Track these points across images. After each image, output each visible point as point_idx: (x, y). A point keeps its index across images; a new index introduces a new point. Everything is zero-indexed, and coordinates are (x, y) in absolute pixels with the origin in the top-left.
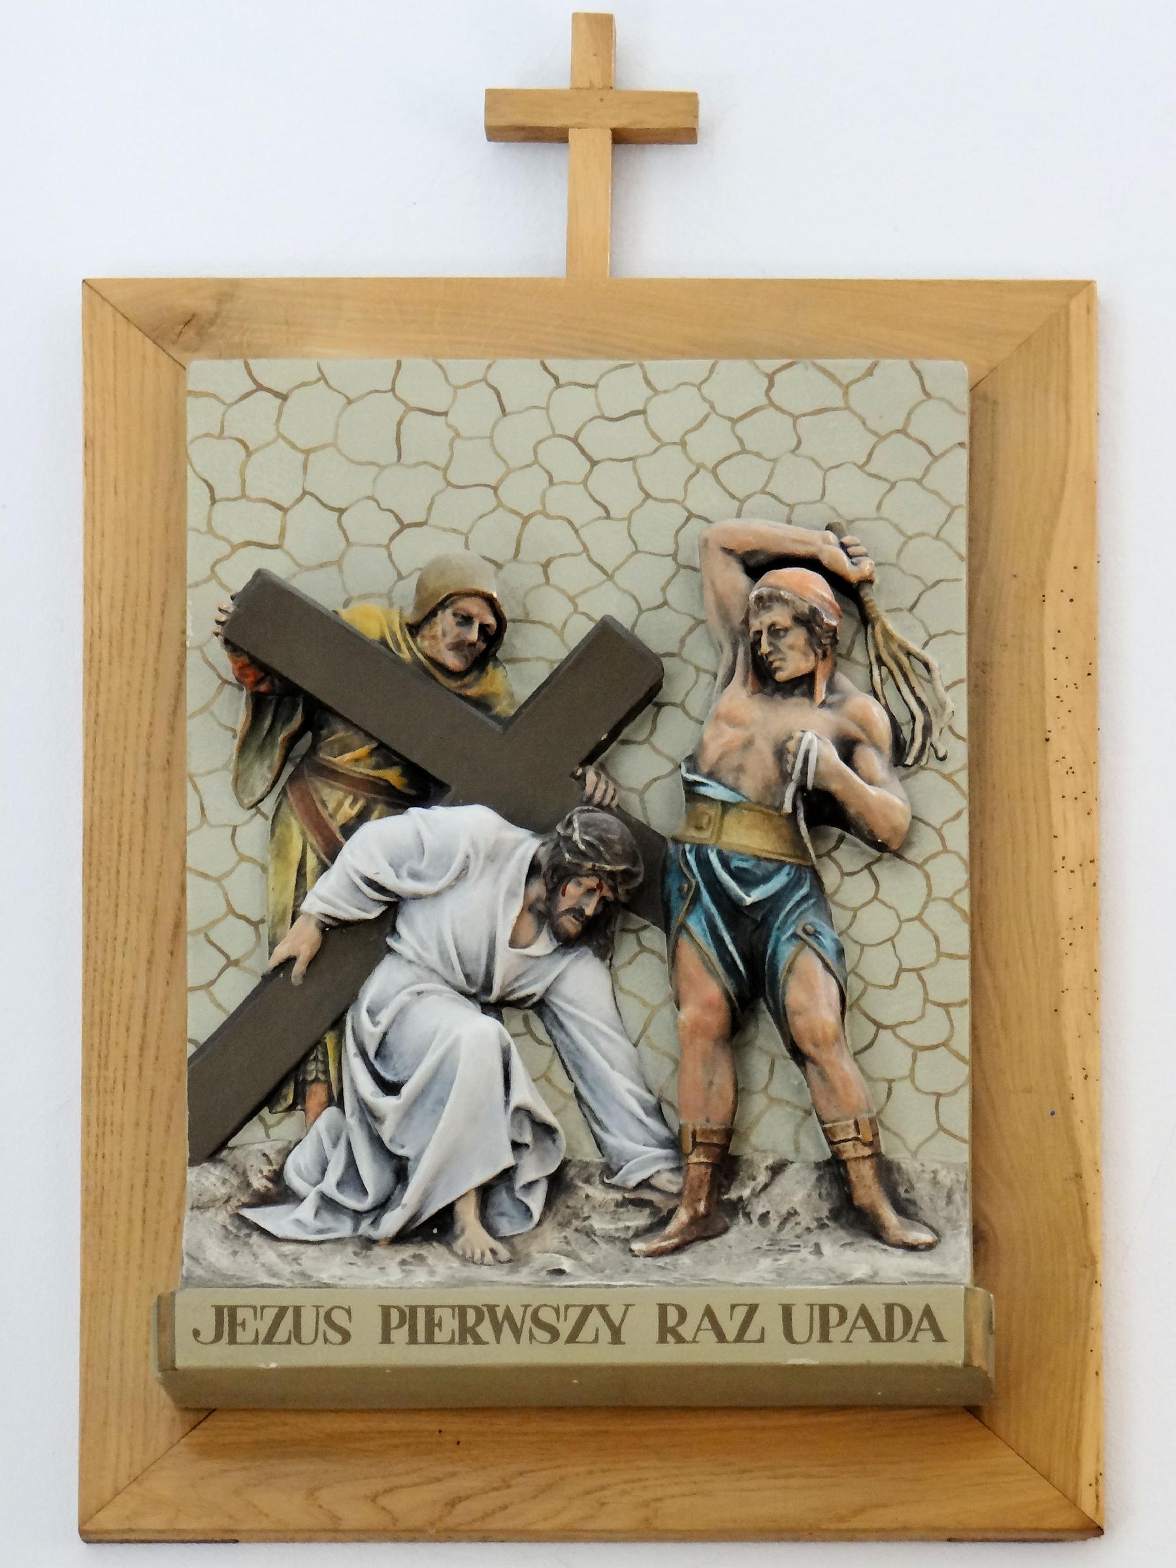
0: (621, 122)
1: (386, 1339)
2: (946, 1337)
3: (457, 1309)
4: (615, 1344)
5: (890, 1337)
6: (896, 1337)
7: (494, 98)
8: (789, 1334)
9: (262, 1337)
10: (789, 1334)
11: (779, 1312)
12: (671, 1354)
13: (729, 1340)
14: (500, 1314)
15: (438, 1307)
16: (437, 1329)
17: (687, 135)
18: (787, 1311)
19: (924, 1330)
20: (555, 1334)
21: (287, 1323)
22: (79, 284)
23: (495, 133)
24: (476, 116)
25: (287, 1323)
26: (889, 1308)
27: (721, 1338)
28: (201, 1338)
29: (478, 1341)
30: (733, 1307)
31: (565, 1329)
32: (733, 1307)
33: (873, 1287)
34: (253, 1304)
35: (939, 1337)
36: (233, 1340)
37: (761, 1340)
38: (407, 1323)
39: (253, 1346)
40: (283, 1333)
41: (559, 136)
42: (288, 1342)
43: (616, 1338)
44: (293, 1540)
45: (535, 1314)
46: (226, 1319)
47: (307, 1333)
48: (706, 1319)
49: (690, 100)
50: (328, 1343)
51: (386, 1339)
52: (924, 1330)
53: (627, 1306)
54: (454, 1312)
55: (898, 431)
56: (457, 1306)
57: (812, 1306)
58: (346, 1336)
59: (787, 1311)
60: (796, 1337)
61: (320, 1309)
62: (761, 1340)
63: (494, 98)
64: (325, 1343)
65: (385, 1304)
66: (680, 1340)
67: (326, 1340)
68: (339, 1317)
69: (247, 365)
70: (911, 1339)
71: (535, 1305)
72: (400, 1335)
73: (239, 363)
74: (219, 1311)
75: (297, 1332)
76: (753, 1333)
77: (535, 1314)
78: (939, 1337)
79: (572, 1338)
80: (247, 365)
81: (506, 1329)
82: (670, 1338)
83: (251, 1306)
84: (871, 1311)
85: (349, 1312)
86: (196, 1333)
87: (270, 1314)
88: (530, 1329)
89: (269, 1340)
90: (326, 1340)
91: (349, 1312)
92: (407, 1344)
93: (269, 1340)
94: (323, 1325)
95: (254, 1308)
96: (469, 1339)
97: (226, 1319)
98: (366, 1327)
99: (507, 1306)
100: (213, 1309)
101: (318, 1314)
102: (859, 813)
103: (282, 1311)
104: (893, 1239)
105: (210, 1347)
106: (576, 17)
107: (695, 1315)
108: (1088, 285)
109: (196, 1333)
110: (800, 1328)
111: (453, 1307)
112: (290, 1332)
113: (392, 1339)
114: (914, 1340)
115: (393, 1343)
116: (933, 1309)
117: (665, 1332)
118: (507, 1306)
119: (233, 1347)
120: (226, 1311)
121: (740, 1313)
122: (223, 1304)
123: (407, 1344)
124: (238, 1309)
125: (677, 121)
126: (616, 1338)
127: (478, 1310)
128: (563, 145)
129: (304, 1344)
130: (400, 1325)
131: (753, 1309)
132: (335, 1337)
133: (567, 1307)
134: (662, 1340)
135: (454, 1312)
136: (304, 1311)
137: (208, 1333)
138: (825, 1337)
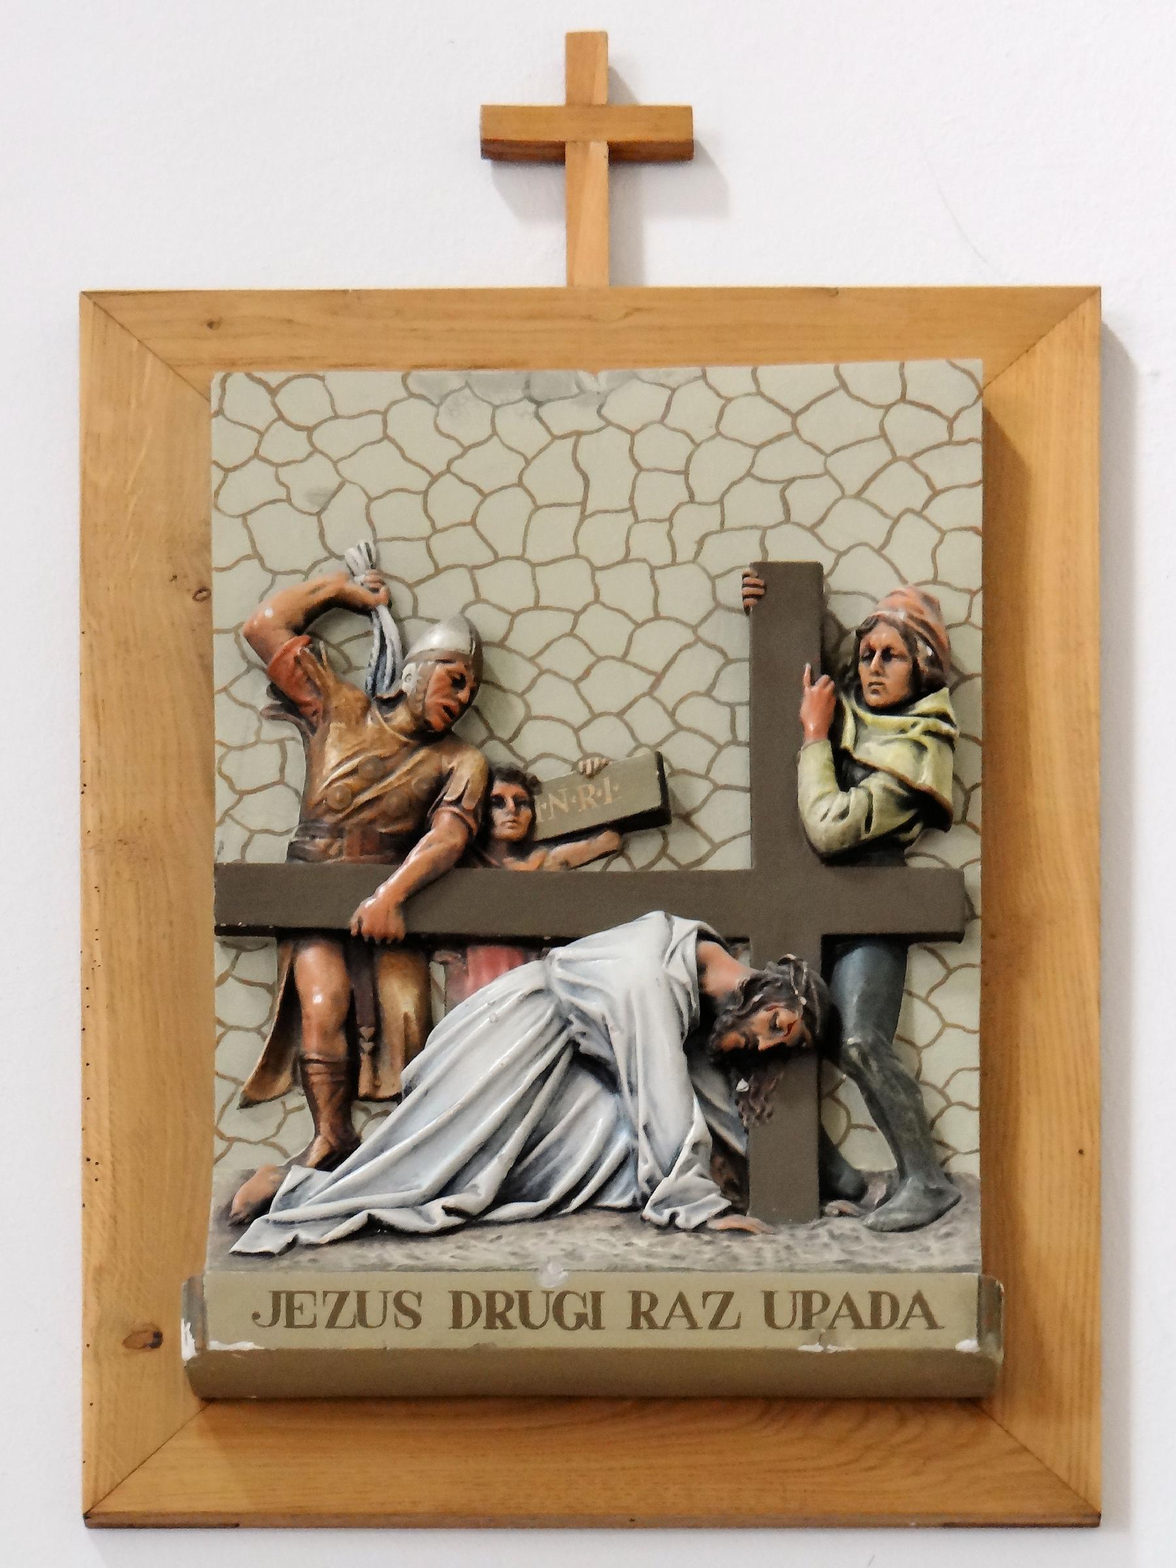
1: (457, 1323)
2: (939, 1321)
5: (876, 1323)
6: (465, 1323)
7: (490, 114)
8: (770, 1319)
10: (770, 1319)
12: (644, 1339)
13: (865, 1325)
18: (769, 1297)
19: (843, 1316)
21: (351, 1305)
22: (71, 311)
25: (351, 1305)
26: (876, 1297)
27: (693, 1325)
29: (507, 1326)
30: (706, 1295)
32: (706, 1295)
33: (734, 1274)
35: (932, 1324)
37: (737, 1326)
42: (353, 1326)
44: (906, 1526)
45: (398, 1299)
47: (373, 1316)
49: (687, 112)
52: (843, 1316)
54: (794, 1298)
55: (291, 505)
57: (794, 1294)
58: (417, 1320)
59: (769, 1297)
60: (778, 1322)
61: (388, 1295)
62: (737, 1326)
63: (490, 114)
64: (397, 1326)
65: (276, 1290)
66: (652, 1325)
67: (397, 1325)
68: (409, 1301)
74: (276, 1296)
75: (361, 1318)
76: (728, 1319)
77: (398, 1299)
78: (932, 1324)
82: (643, 1322)
85: (419, 1297)
86: (256, 1316)
90: (397, 1325)
91: (419, 1297)
94: (391, 1308)
96: (498, 1323)
98: (436, 1311)
100: (450, 1296)
101: (385, 1298)
103: (343, 1297)
107: (666, 1303)
108: (1094, 293)
110: (782, 1314)
114: (903, 1327)
115: (604, 1328)
116: (927, 1297)
117: (639, 1317)
118: (847, 1293)
120: (283, 1297)
121: (715, 1302)
123: (484, 1328)
124: (642, 1294)
125: (669, 134)
129: (779, 1328)
131: (728, 1297)
132: (407, 1321)
133: (325, 1294)
134: (635, 1325)
135: (794, 1298)
136: (531, 1297)
137: (267, 1315)
138: (807, 1324)
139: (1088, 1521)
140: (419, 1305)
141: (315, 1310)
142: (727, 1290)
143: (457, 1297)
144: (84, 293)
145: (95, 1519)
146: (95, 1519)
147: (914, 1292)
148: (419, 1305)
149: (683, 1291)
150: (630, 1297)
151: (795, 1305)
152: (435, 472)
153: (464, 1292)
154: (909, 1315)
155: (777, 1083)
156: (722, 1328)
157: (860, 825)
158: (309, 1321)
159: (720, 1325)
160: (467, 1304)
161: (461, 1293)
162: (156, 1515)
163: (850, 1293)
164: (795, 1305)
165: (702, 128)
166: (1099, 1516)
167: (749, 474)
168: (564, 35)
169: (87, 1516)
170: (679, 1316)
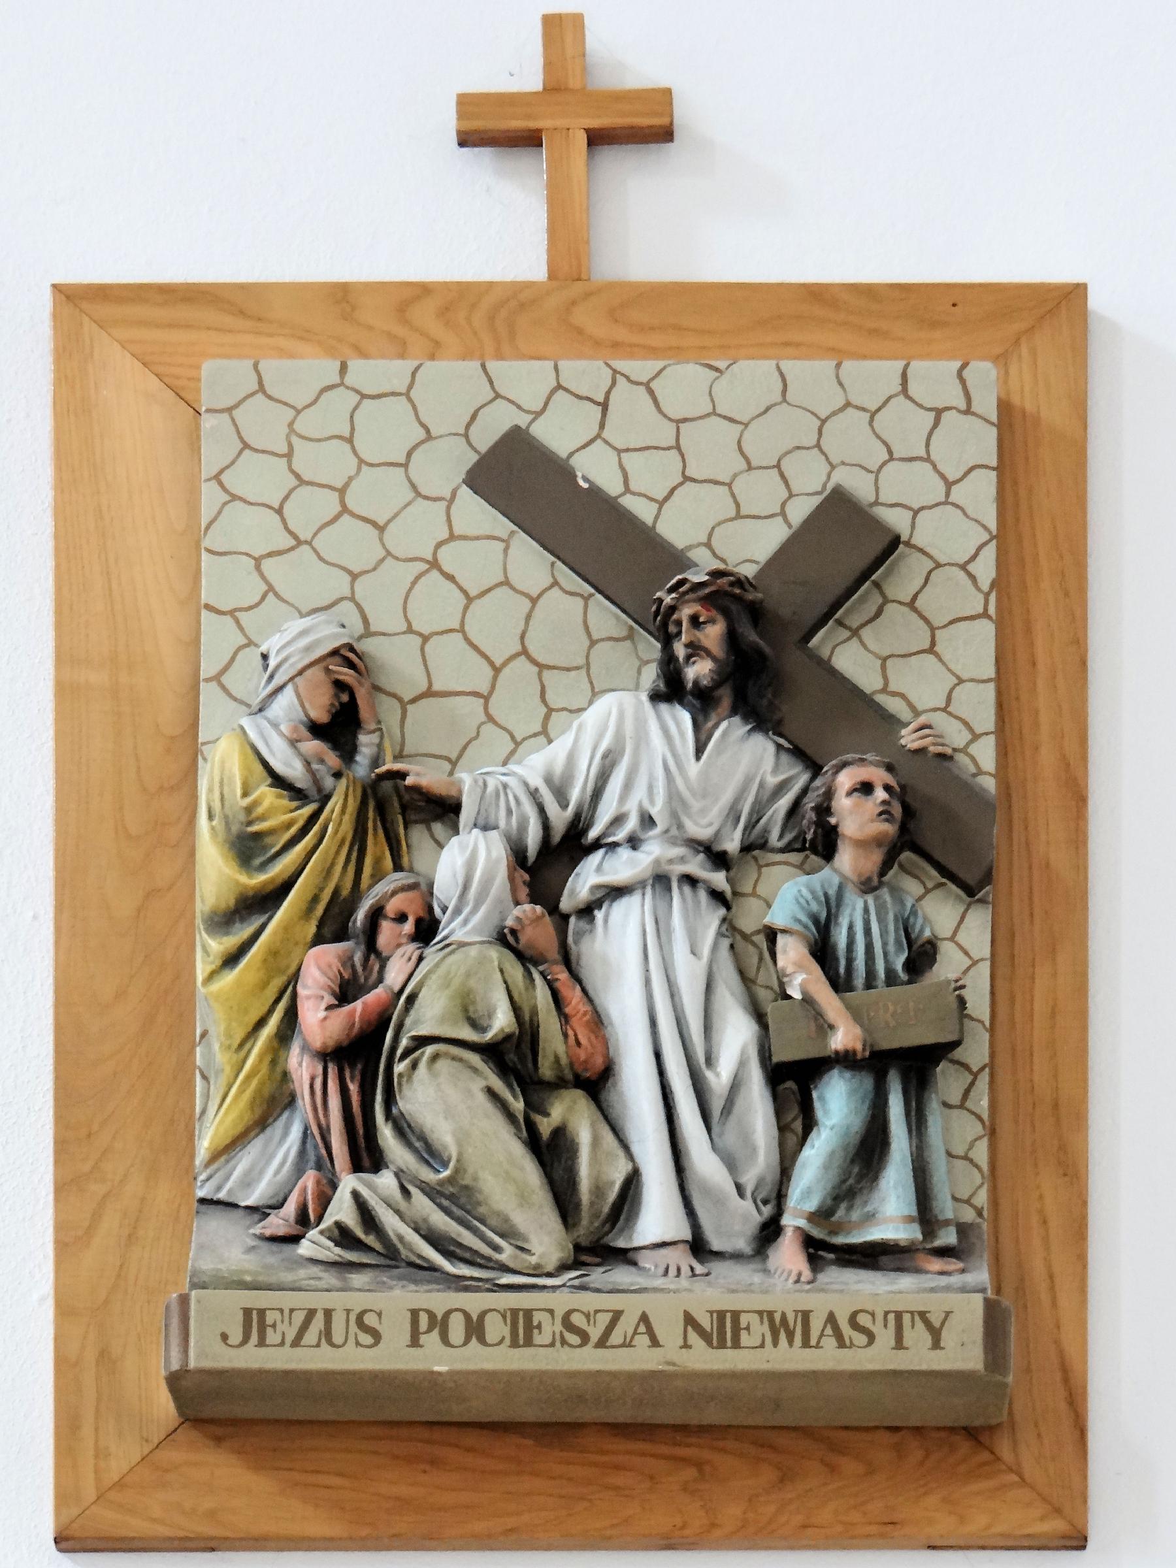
0: (595, 123)
1: (415, 1342)
2: (661, 1338)
3: (800, 1314)
4: (514, 1348)
5: (722, 1345)
7: (467, 104)
9: (289, 1340)
11: (240, 1316)
12: (251, 1358)
14: (777, 1317)
15: (744, 1312)
16: (536, 1331)
17: (666, 134)
20: (585, 1337)
21: (318, 1323)
22: (45, 301)
23: (462, 144)
24: (448, 123)
25: (318, 1323)
28: (230, 1342)
31: (595, 1333)
34: (585, 1310)
35: (655, 1343)
36: (262, 1343)
38: (438, 1325)
39: (550, 1349)
40: (311, 1336)
41: (531, 140)
43: (936, 1345)
45: (360, 1317)
46: (521, 1321)
48: (829, 1326)
49: (666, 95)
50: (565, 1346)
51: (415, 1342)
53: (948, 1314)
54: (712, 1316)
56: (716, 1311)
57: (711, 1312)
58: (376, 1336)
63: (467, 104)
68: (370, 1320)
69: (483, 366)
70: (256, 1343)
71: (358, 1310)
72: (431, 1340)
73: (476, 365)
74: (247, 1312)
75: (327, 1333)
77: (360, 1317)
78: (655, 1343)
79: (602, 1343)
80: (483, 366)
81: (783, 1336)
83: (277, 1309)
84: (695, 1315)
85: (380, 1315)
86: (224, 1337)
87: (299, 1317)
88: (356, 1334)
89: (296, 1343)
90: (358, 1344)
91: (380, 1315)
92: (649, 1347)
93: (296, 1343)
95: (281, 1311)
97: (521, 1321)
98: (670, 1330)
99: (685, 1311)
100: (241, 1312)
102: (225, 841)
103: (311, 1313)
104: (681, 1246)
105: (578, 1350)
106: (666, 95)
109: (224, 1337)
111: (760, 1313)
112: (321, 1331)
113: (421, 1342)
117: (475, 1329)
118: (685, 1311)
119: (263, 1350)
122: (724, 1308)
126: (936, 1345)
127: (912, 1313)
128: (532, 151)
130: (429, 1330)
132: (367, 1339)
133: (292, 1311)
135: (712, 1316)
137: (236, 1337)
139: (1075, 1543)
140: (380, 1323)
141: (495, 1328)
142: (617, 1308)
143: (415, 1314)
144: (54, 286)
145: (65, 1541)
146: (65, 1541)
147: (640, 1313)
148: (380, 1323)
149: (834, 1311)
150: (409, 1314)
151: (712, 1320)
152: (241, 446)
153: (421, 1310)
154: (822, 1335)
155: (204, 1077)
156: (268, 1346)
157: (582, 809)
158: (548, 1341)
159: (302, 1344)
160: (424, 1319)
161: (265, 1310)
162: (140, 1539)
163: (687, 1309)
164: (712, 1320)
165: (683, 114)
166: (1086, 1539)
167: (298, 412)
168: (540, 16)
169: (57, 1541)
170: (643, 1333)
